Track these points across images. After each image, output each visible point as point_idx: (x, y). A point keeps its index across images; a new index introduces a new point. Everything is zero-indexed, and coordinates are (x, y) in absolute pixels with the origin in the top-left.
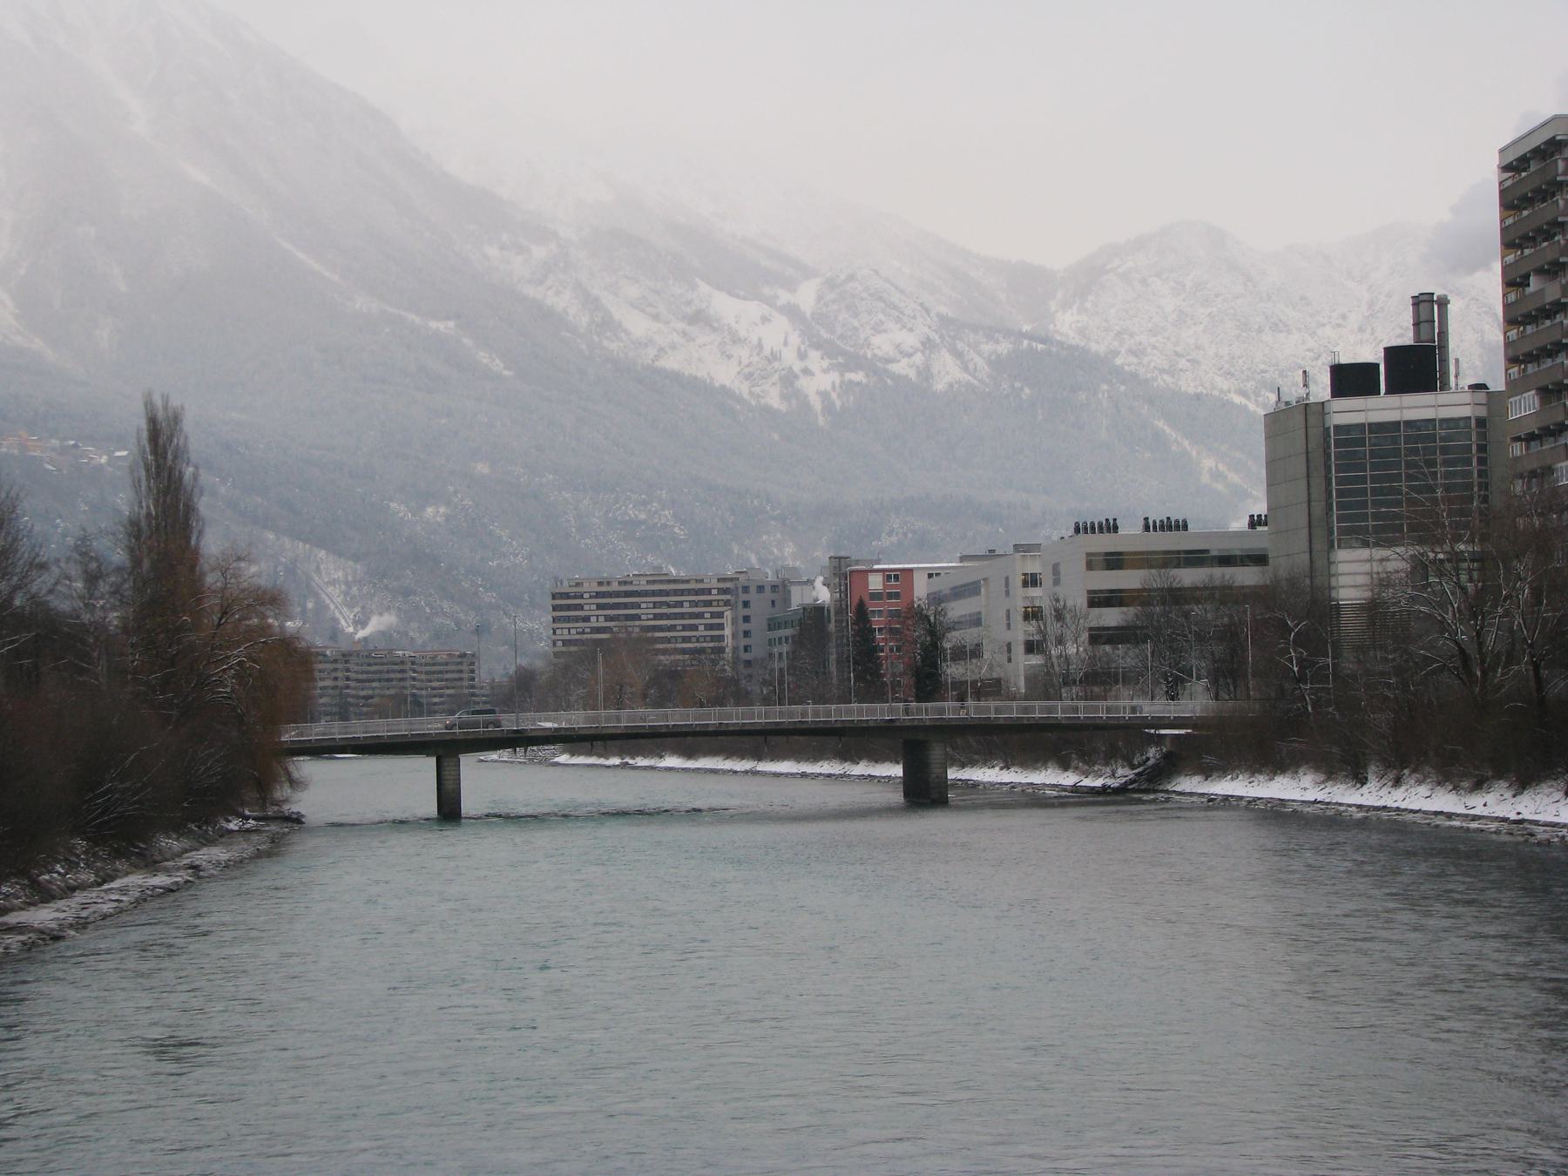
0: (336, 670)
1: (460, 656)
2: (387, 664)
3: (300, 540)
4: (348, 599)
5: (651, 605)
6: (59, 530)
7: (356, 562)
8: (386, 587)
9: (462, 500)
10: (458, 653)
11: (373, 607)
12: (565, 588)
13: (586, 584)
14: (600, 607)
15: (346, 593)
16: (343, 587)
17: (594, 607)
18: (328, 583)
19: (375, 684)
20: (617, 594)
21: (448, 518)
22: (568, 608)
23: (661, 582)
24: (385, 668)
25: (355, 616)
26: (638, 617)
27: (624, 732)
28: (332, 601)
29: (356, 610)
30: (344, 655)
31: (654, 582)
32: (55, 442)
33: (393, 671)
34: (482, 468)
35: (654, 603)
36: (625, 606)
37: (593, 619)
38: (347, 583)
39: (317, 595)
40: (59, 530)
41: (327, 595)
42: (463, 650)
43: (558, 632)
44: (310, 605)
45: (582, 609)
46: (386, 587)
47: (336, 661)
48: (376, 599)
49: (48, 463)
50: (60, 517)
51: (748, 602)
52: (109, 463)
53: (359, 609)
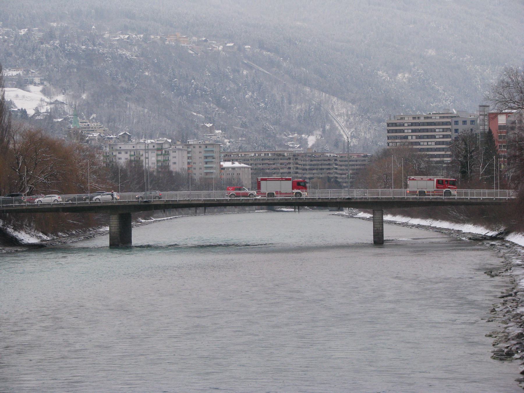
0: (290, 163)
1: (364, 157)
2: (321, 160)
3: (323, 91)
4: (348, 124)
5: (442, 130)
6: (193, 86)
7: (353, 104)
8: (369, 118)
9: (418, 70)
10: (363, 155)
11: (361, 128)
12: (393, 121)
13: (406, 119)
14: (413, 131)
15: (347, 121)
16: (346, 118)
17: (410, 131)
18: (337, 115)
19: (315, 171)
20: (423, 124)
21: (410, 80)
22: (396, 131)
23: (447, 117)
24: (320, 162)
25: (351, 133)
26: (434, 137)
27: (203, 203)
28: (340, 125)
29: (352, 130)
30: (294, 156)
31: (444, 117)
32: (195, 39)
33: (325, 165)
34: (431, 52)
35: (443, 129)
36: (427, 130)
37: (410, 138)
38: (347, 115)
39: (331, 122)
40: (193, 86)
41: (337, 122)
42: (365, 153)
43: (390, 144)
44: (327, 127)
45: (404, 132)
46: (369, 118)
47: (290, 159)
48: (363, 124)
49: (190, 50)
50: (194, 79)
51: (458, 129)
52: (223, 50)
53: (354, 129)
